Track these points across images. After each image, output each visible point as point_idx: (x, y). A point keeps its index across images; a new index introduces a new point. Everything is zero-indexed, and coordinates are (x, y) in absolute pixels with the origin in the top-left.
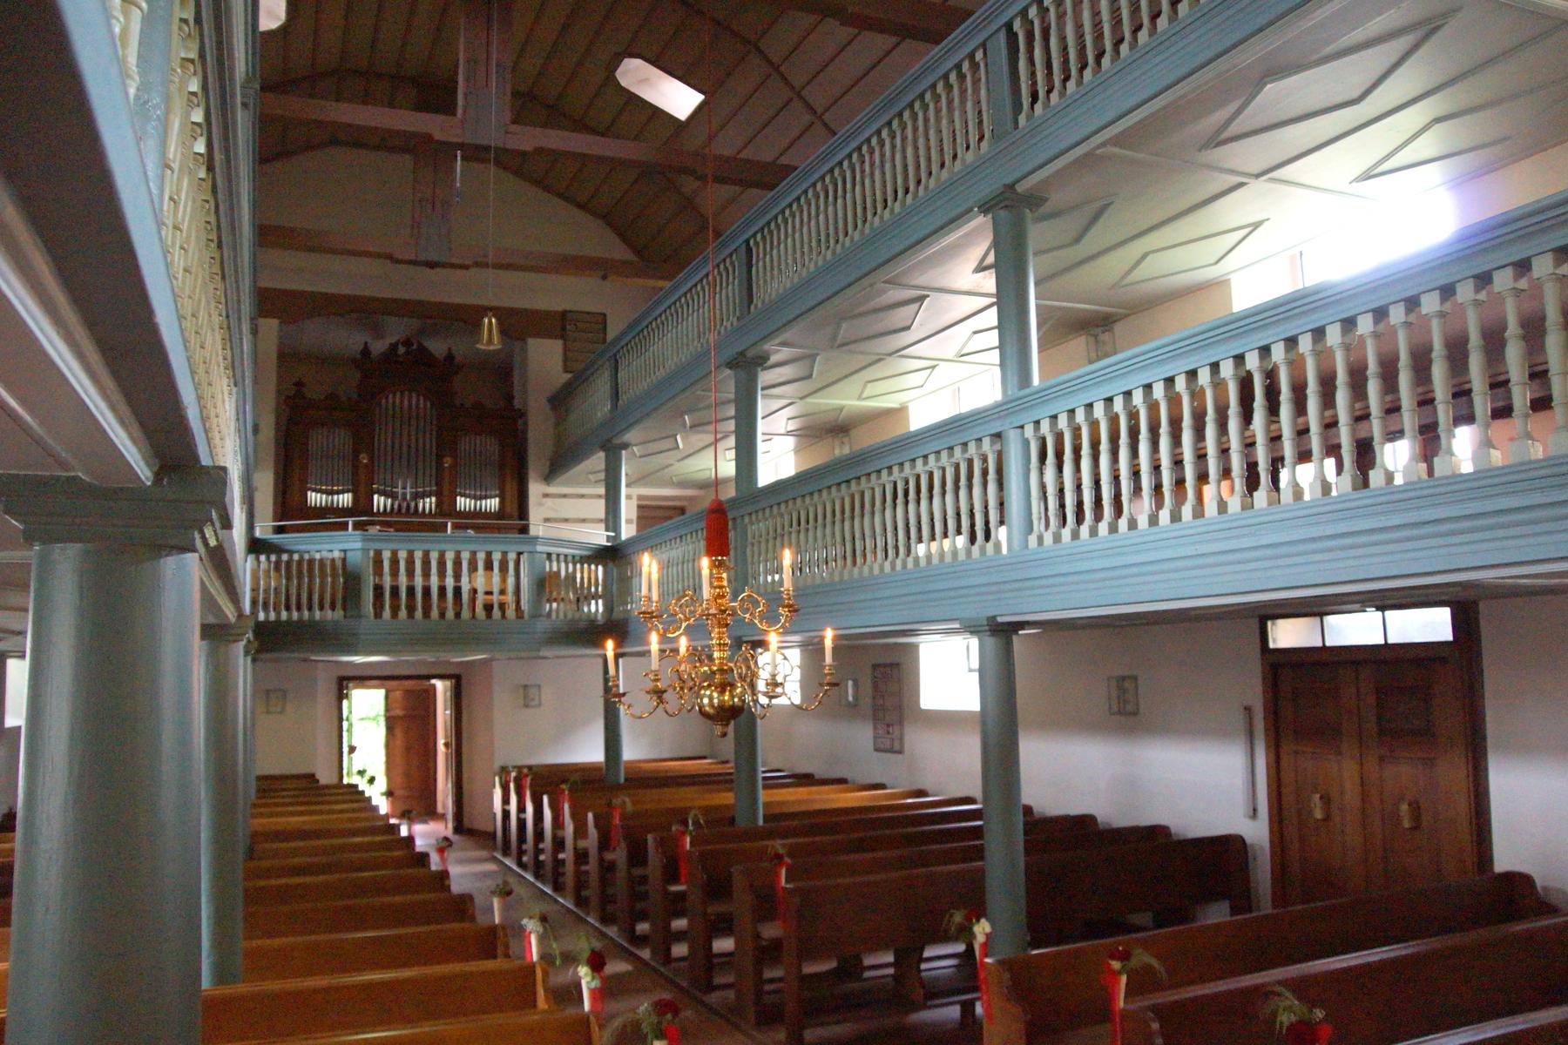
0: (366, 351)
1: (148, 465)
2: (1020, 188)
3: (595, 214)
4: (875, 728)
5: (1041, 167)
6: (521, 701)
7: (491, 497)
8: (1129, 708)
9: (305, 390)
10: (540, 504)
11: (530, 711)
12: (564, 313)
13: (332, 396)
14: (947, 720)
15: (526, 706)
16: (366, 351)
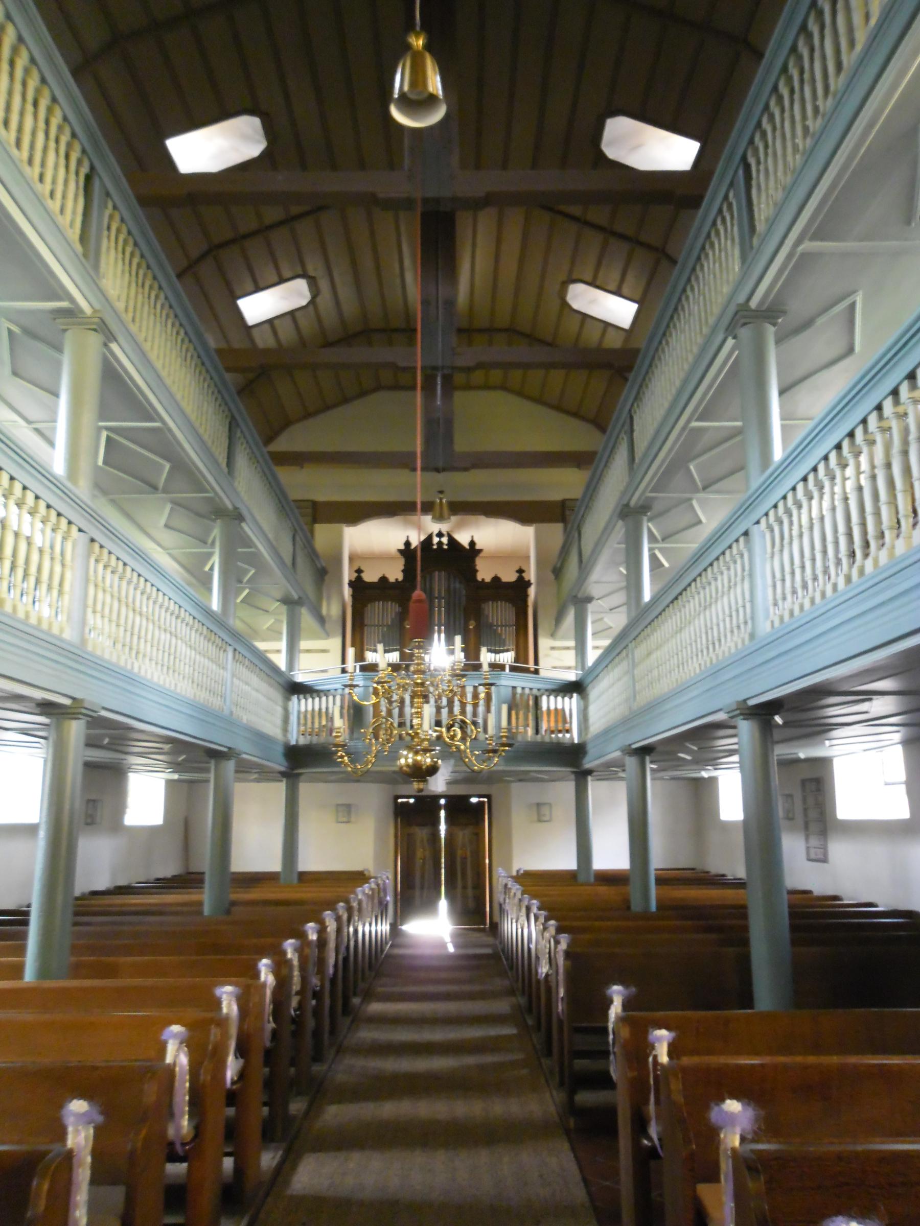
0: (408, 544)
1: (301, 614)
2: (633, 503)
3: (584, 419)
4: (807, 839)
5: (854, 397)
6: (535, 818)
7: (508, 651)
8: (790, 815)
9: (363, 575)
10: (547, 655)
11: (540, 824)
12: (564, 502)
13: (384, 579)
14: (727, 826)
15: (540, 821)
16: (408, 544)
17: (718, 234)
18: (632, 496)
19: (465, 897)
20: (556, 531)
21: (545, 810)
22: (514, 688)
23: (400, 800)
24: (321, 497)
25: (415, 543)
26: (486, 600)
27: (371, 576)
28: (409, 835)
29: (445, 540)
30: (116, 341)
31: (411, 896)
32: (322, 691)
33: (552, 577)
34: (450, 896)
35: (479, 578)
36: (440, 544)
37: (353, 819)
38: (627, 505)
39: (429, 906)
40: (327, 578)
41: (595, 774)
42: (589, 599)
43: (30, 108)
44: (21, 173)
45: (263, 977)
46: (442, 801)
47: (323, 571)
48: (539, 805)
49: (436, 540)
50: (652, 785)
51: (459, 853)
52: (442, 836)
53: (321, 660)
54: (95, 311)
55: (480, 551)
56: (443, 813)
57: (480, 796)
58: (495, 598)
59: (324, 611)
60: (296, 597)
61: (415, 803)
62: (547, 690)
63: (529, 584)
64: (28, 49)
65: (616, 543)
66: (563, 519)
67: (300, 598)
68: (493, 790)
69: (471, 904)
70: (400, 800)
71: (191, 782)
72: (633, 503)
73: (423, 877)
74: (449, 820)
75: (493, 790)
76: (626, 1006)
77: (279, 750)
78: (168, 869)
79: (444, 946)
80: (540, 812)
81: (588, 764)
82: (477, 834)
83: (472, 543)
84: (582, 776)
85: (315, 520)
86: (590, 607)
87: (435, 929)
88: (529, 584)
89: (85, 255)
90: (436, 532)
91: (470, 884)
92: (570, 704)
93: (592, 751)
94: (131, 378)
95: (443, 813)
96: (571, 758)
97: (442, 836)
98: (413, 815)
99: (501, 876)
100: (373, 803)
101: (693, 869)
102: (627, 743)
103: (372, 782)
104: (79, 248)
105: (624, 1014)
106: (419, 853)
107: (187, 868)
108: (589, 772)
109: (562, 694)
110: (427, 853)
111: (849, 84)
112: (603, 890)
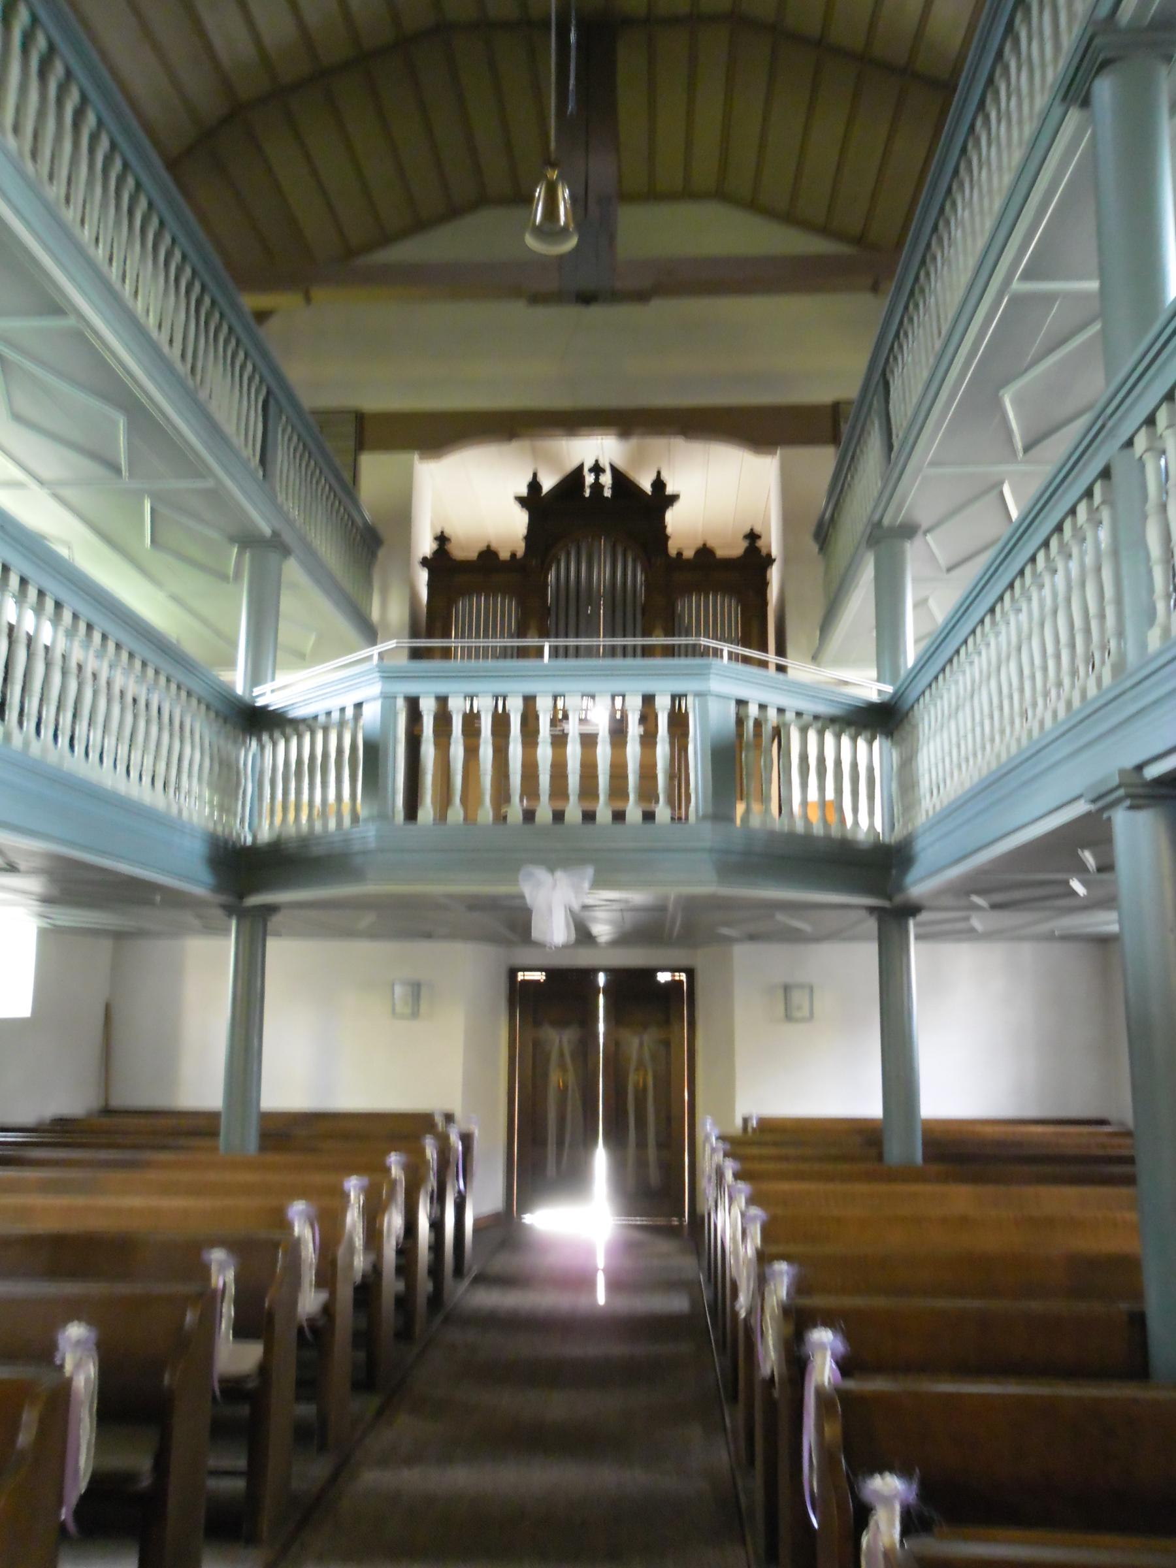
0: (534, 486)
15: (789, 1017)
19: (642, 1163)
20: (820, 461)
21: (798, 997)
22: (741, 703)
23: (521, 976)
24: (374, 402)
25: (548, 484)
26: (688, 589)
27: (465, 549)
29: (606, 479)
31: (539, 1159)
32: (304, 720)
33: (814, 548)
35: (672, 550)
39: (573, 1179)
40: (381, 553)
41: (924, 916)
42: (908, 531)
45: (297, 1230)
46: (601, 979)
47: (370, 541)
48: (787, 989)
49: (590, 479)
51: (632, 1078)
52: (603, 1045)
53: (337, 683)
55: (674, 498)
57: (673, 970)
58: (702, 588)
59: (375, 615)
60: (267, 531)
62: (816, 717)
63: (769, 560)
66: (834, 439)
67: (275, 534)
68: (700, 959)
69: (654, 1176)
71: (119, 936)
73: (562, 1119)
74: (615, 1016)
75: (700, 959)
77: (194, 851)
78: (69, 1099)
79: (585, 1282)
80: (790, 1002)
81: (920, 885)
82: (667, 1044)
83: (659, 484)
84: (894, 918)
85: (361, 445)
86: (912, 550)
87: (584, 1226)
88: (769, 560)
90: (588, 464)
92: (869, 753)
93: (927, 853)
96: (873, 877)
97: (603, 1045)
98: (548, 1002)
99: (709, 1129)
100: (466, 977)
101: (1102, 1122)
102: (1130, 762)
103: (452, 936)
106: (555, 1078)
107: (107, 1099)
108: (913, 910)
109: (853, 730)
110: (571, 1078)
112: (961, 1198)
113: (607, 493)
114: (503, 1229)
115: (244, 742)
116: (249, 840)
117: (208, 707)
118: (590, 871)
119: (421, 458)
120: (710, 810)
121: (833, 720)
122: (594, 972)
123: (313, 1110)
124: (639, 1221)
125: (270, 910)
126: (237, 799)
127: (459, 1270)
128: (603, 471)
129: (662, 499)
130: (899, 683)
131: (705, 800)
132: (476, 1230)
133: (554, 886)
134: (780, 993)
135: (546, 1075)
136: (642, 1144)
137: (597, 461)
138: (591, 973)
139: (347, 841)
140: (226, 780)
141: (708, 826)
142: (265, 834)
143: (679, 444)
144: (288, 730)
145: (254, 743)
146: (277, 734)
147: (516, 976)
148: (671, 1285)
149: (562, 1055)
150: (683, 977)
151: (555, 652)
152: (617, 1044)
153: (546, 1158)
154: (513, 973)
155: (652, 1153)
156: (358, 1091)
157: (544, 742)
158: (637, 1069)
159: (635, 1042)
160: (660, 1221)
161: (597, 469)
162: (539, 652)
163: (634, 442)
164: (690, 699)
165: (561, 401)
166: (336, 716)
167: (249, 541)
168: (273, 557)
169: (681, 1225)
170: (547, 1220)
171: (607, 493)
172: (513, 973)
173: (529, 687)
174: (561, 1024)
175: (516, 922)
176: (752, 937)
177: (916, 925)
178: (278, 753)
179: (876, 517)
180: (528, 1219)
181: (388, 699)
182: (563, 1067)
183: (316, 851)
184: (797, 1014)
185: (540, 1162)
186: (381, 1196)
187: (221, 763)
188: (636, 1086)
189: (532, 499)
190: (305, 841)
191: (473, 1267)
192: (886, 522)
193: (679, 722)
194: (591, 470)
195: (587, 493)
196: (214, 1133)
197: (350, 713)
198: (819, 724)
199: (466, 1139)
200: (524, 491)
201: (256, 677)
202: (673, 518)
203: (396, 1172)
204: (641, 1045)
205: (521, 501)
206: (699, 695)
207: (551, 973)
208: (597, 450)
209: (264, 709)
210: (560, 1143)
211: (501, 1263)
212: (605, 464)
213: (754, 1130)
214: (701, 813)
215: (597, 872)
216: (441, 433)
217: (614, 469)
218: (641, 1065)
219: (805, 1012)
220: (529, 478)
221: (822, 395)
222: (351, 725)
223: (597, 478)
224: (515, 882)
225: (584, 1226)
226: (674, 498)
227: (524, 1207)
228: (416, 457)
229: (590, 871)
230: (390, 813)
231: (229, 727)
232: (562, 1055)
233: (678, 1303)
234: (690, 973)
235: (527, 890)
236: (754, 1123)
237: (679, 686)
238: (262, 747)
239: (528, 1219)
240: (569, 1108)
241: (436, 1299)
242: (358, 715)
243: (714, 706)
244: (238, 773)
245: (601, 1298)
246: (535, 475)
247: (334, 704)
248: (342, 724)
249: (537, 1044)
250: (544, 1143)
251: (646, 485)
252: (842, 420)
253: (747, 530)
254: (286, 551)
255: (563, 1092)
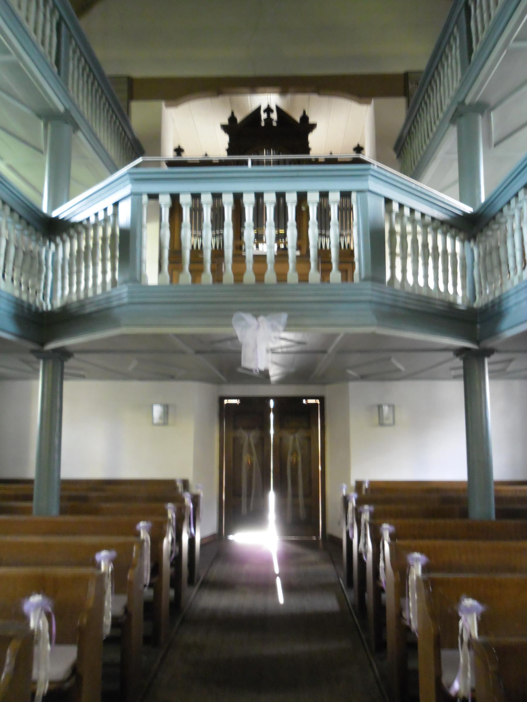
0: (232, 119)
12: (406, 76)
15: (381, 424)
17: (423, 109)
18: (466, 95)
19: (295, 506)
20: (397, 108)
23: (226, 402)
24: (138, 72)
25: (239, 118)
28: (235, 439)
29: (274, 116)
30: (81, 130)
33: (395, 156)
34: (280, 488)
36: (269, 120)
37: (170, 420)
38: (463, 103)
39: (255, 516)
43: (76, 69)
44: (29, 37)
45: (32, 624)
46: (272, 403)
49: (264, 116)
50: (490, 386)
51: (290, 459)
54: (66, 109)
56: (272, 416)
61: (304, 404)
64: (75, 40)
65: (449, 143)
66: (406, 93)
68: (327, 391)
69: (302, 513)
70: (226, 402)
72: (467, 101)
75: (327, 391)
76: (426, 569)
79: (270, 563)
82: (309, 439)
83: (305, 118)
85: (131, 97)
89: (59, 73)
90: (264, 107)
91: (301, 492)
94: (31, 72)
95: (272, 416)
98: (241, 417)
100: (195, 400)
104: (55, 69)
105: (425, 576)
106: (246, 459)
110: (255, 459)
111: (482, 49)
113: (275, 124)
114: (217, 544)
115: (44, 244)
116: (49, 308)
117: (12, 210)
118: (284, 317)
119: (167, 106)
120: (370, 274)
121: (443, 222)
122: (268, 399)
123: (108, 479)
124: (293, 538)
125: (64, 354)
126: (39, 279)
127: (191, 581)
128: (272, 111)
129: (306, 126)
130: (478, 206)
131: (366, 267)
132: (202, 545)
133: (258, 327)
134: (376, 409)
135: (241, 455)
136: (295, 495)
137: (268, 106)
138: (265, 400)
139: (108, 299)
140: (30, 265)
141: (369, 285)
142: (58, 303)
143: (314, 98)
144: (72, 232)
145: (53, 246)
146: (65, 236)
147: (223, 402)
148: (323, 587)
149: (249, 445)
150: (318, 402)
151: (254, 163)
152: (281, 439)
153: (241, 502)
154: (221, 399)
155: (301, 500)
156: (133, 467)
157: (249, 226)
158: (292, 454)
159: (291, 438)
160: (305, 538)
161: (269, 110)
162: (245, 163)
163: (289, 97)
164: (354, 196)
165: (248, 72)
166: (101, 217)
167: (49, 116)
168: (67, 128)
169: (318, 540)
170: (242, 538)
171: (275, 124)
172: (221, 399)
173: (238, 187)
174: (249, 428)
175: (227, 363)
176: (363, 377)
177: (489, 364)
178: (64, 249)
179: (460, 99)
180: (231, 537)
181: (135, 195)
182: (251, 453)
183: (89, 309)
184: (386, 422)
185: (238, 507)
186: (132, 555)
187: (25, 253)
188: (292, 463)
189: (230, 127)
190: (82, 303)
191: (201, 573)
192: (467, 101)
193: (345, 211)
194: (265, 111)
195: (263, 124)
196: (29, 498)
197: (110, 212)
198: (435, 224)
199: (195, 499)
200: (226, 122)
201: (55, 204)
202: (313, 139)
203: (144, 535)
204: (295, 439)
205: (225, 128)
206: (359, 191)
207: (243, 399)
208: (268, 100)
209: (57, 218)
210: (249, 496)
211: (218, 571)
212: (274, 108)
213: (366, 490)
214: (363, 276)
215: (289, 318)
216: (179, 90)
217: (278, 108)
218: (295, 451)
219: (391, 421)
220: (229, 114)
221: (398, 68)
222: (111, 219)
223: (269, 115)
224: (230, 325)
225: (263, 540)
226: (313, 126)
227: (229, 531)
228: (163, 104)
229: (284, 317)
230: (138, 277)
231: (31, 228)
232: (249, 445)
233: (328, 603)
234: (322, 399)
235: (238, 332)
236: (366, 485)
237: (346, 186)
238: (57, 246)
239: (231, 537)
240: (254, 476)
241: (176, 604)
242: (115, 214)
243: (371, 199)
244: (40, 263)
245: (281, 599)
246: (233, 113)
247: (99, 207)
248: (106, 220)
249: (235, 439)
250: (240, 495)
251: (298, 119)
252: (410, 82)
253: (355, 145)
254: (76, 127)
255: (251, 467)
